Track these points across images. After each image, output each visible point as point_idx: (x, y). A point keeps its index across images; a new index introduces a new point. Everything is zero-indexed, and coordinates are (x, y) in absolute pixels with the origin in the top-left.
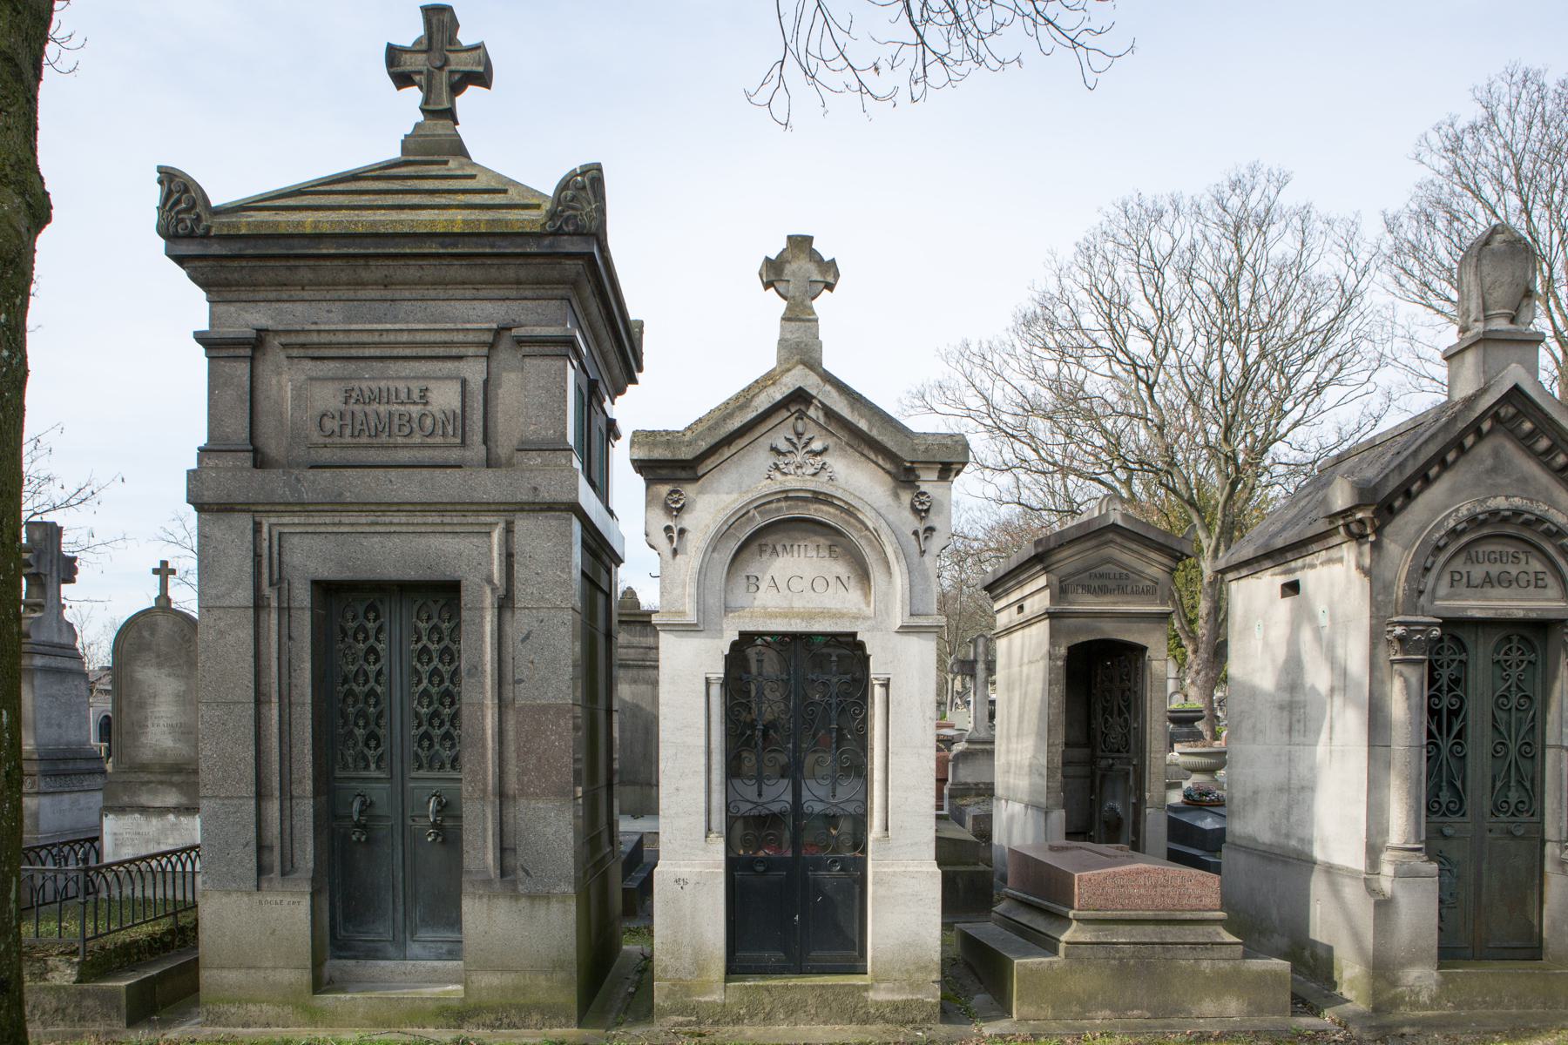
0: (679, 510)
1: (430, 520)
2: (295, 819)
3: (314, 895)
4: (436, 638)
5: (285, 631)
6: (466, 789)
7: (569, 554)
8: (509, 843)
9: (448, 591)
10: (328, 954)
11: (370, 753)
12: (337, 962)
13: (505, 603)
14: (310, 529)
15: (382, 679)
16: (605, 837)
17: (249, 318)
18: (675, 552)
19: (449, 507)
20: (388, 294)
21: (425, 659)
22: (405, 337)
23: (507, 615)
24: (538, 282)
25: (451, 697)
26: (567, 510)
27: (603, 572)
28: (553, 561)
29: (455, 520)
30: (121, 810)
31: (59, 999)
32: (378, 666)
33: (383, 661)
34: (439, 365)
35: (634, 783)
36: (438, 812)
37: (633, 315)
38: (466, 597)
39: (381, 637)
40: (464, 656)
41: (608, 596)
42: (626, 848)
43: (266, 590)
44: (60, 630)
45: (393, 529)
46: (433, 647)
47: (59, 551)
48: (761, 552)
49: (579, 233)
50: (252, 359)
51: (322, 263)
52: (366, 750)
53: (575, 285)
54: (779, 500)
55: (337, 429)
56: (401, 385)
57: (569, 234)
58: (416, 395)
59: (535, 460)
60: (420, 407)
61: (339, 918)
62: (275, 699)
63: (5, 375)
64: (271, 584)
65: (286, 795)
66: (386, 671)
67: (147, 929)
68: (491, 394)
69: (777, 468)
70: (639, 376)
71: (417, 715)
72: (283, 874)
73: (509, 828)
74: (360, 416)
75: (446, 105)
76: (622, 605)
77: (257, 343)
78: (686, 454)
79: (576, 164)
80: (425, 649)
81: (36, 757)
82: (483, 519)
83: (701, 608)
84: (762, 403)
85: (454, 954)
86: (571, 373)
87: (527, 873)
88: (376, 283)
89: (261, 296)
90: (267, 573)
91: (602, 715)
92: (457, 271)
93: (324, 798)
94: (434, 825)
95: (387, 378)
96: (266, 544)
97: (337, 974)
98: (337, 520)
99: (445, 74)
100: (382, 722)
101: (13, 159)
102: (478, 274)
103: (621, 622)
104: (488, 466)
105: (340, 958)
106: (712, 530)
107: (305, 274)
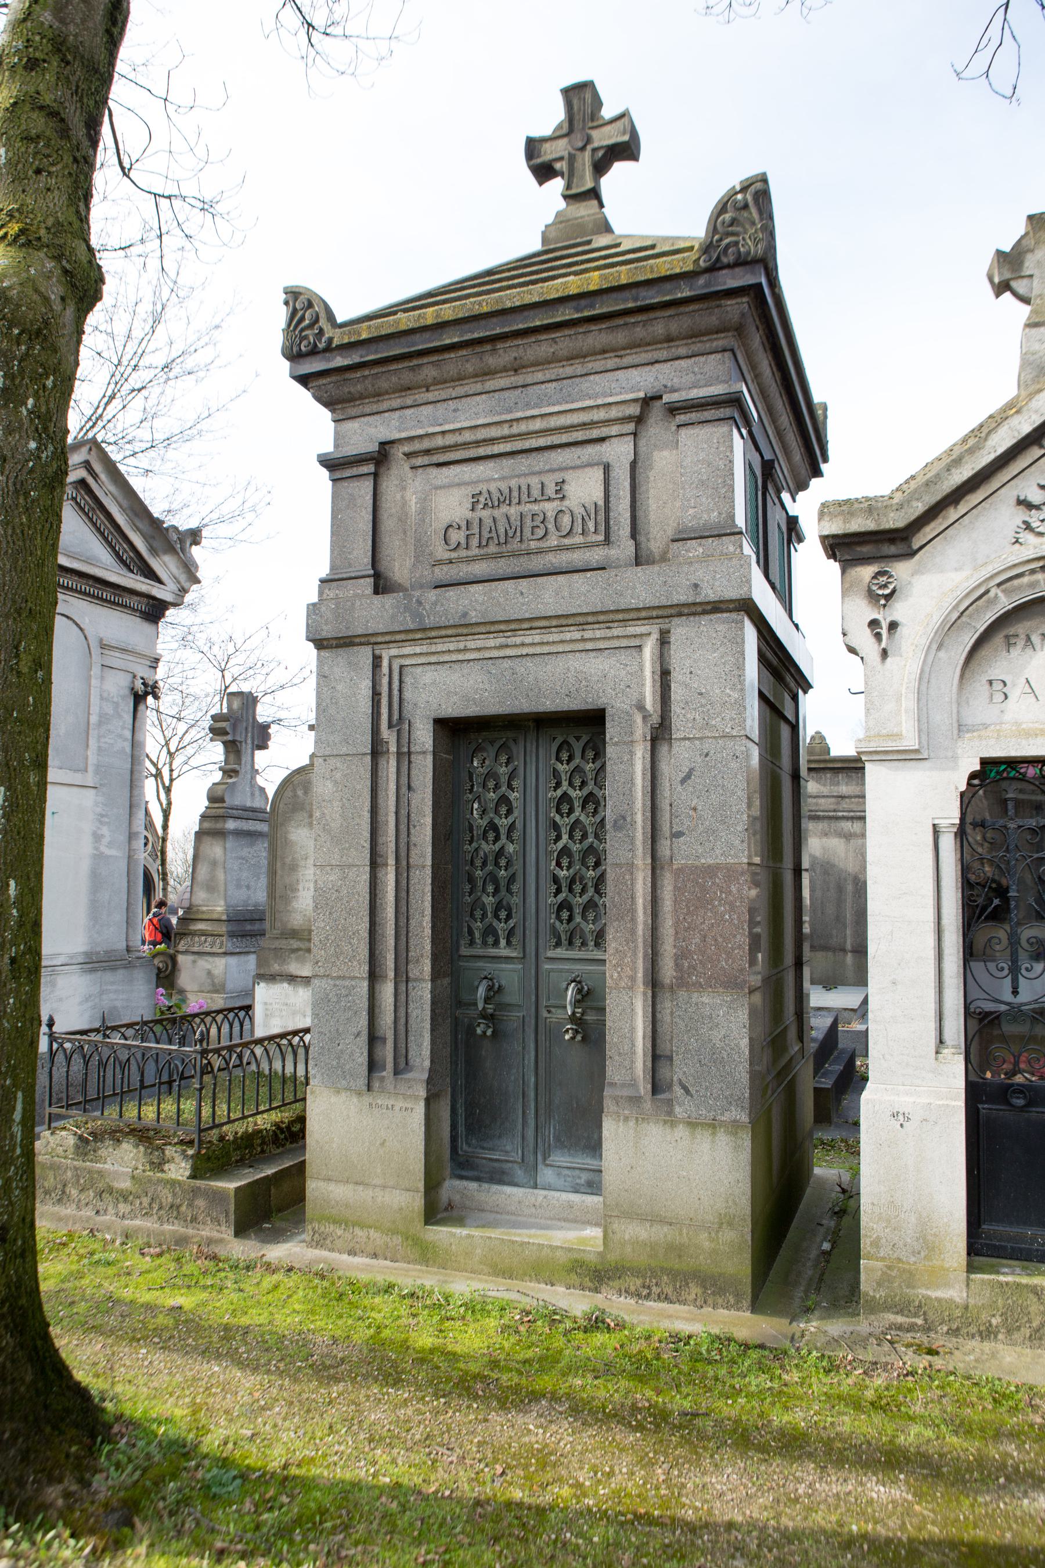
0: (888, 597)
1: (568, 636)
2: (411, 1006)
3: (430, 1101)
4: (577, 782)
5: (404, 780)
6: (611, 974)
7: (740, 667)
8: (664, 1048)
9: (593, 721)
10: (448, 1172)
11: (501, 927)
12: (457, 1183)
13: (660, 734)
14: (433, 659)
15: (516, 835)
16: (792, 1033)
17: (367, 433)
18: (885, 653)
19: (590, 619)
20: (519, 379)
21: (565, 808)
22: (538, 425)
23: (663, 749)
24: (694, 335)
25: (595, 856)
26: (737, 610)
27: (787, 698)
28: (719, 672)
29: (598, 634)
30: (272, 978)
31: (174, 1195)
32: (510, 819)
33: (516, 813)
34: (577, 451)
35: (825, 948)
36: (577, 1003)
37: (817, 398)
38: (612, 730)
39: (514, 783)
40: (610, 804)
41: (795, 728)
42: (819, 1025)
43: (386, 733)
44: (253, 795)
45: (525, 651)
46: (574, 794)
47: (254, 718)
48: (1009, 645)
49: (743, 262)
50: (376, 475)
51: (447, 356)
52: (495, 923)
53: (739, 330)
54: (1033, 572)
55: (463, 541)
56: (534, 481)
57: (729, 266)
58: (550, 491)
59: (696, 549)
60: (556, 503)
61: (461, 1129)
62: (391, 861)
63: (32, 471)
64: (390, 726)
65: (402, 977)
66: (519, 825)
67: (275, 1116)
68: (640, 478)
69: (1028, 527)
70: (824, 467)
71: (556, 880)
72: (396, 1072)
73: (664, 1029)
74: (488, 522)
75: (589, 185)
76: (810, 751)
77: (380, 457)
78: (895, 521)
79: (735, 181)
80: (565, 797)
81: (224, 917)
82: (631, 630)
83: (924, 728)
84: (1002, 441)
85: (594, 1187)
86: (738, 444)
87: (687, 1091)
88: (505, 369)
89: (385, 405)
90: (387, 708)
91: (788, 877)
92: (597, 337)
93: (446, 981)
94: (573, 1019)
95: (519, 476)
96: (385, 681)
97: (457, 1198)
98: (461, 646)
99: (587, 154)
100: (515, 888)
101: (50, 221)
102: (620, 337)
103: (810, 769)
104: (638, 563)
105: (462, 1178)
106: (937, 619)
107: (429, 372)
